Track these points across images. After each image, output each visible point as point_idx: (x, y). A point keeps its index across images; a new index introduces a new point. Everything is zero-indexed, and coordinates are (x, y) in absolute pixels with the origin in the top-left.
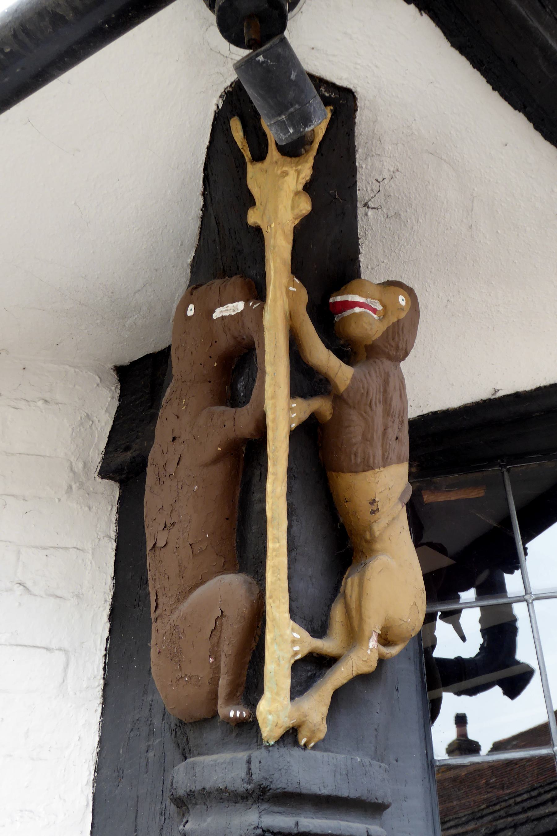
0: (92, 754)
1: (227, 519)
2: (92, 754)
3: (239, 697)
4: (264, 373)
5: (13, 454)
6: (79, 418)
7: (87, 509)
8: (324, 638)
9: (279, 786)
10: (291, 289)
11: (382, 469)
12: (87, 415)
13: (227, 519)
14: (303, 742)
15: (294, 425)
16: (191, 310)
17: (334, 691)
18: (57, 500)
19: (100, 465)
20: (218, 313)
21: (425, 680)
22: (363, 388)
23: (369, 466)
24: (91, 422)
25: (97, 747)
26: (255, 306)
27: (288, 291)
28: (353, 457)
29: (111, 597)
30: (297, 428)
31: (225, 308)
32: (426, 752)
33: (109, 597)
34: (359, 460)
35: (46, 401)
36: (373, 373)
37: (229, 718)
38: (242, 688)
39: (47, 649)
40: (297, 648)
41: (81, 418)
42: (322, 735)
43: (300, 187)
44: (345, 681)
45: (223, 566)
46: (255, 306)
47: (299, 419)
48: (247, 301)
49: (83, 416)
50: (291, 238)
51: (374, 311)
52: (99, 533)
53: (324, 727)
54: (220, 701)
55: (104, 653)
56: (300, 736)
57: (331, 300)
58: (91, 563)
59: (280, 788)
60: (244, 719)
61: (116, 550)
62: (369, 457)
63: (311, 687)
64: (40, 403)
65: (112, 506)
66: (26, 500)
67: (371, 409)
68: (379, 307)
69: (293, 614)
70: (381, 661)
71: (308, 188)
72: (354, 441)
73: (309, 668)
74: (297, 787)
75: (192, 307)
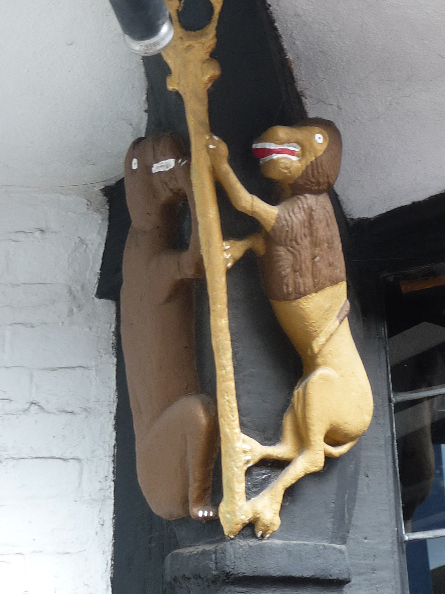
0: (109, 546)
1: (186, 348)
2: (109, 546)
3: (208, 499)
4: (197, 223)
5: (18, 285)
6: (73, 244)
7: (88, 329)
8: (277, 445)
9: (239, 572)
10: (211, 146)
11: (314, 294)
12: (81, 239)
13: (186, 348)
14: (259, 534)
15: (230, 265)
16: (135, 164)
17: (285, 490)
18: (60, 324)
19: (97, 286)
20: (156, 168)
21: (397, 465)
22: (288, 226)
23: (300, 294)
24: (85, 246)
25: (113, 540)
26: (183, 164)
27: (208, 149)
28: (285, 287)
29: (115, 408)
30: (233, 267)
31: (160, 164)
32: (396, 529)
33: (113, 408)
34: (291, 289)
35: (42, 231)
36: (296, 210)
37: (199, 517)
38: (210, 492)
39: (64, 460)
40: (248, 457)
41: (75, 243)
42: (276, 528)
43: (207, 56)
44: (293, 482)
45: (186, 389)
46: (183, 164)
47: (234, 259)
48: (177, 159)
49: (77, 242)
50: (206, 101)
51: (292, 153)
52: (101, 351)
53: (277, 521)
54: (191, 504)
55: (112, 459)
56: (256, 530)
57: (254, 146)
58: (95, 379)
59: (241, 573)
60: (211, 517)
61: (117, 365)
62: (299, 286)
63: (267, 487)
64: (37, 234)
65: (111, 324)
66: (34, 327)
67: (298, 244)
68: (297, 150)
69: (244, 427)
70: (329, 459)
71: (214, 55)
72: (283, 273)
73: (263, 472)
74: (255, 572)
75: (135, 161)
